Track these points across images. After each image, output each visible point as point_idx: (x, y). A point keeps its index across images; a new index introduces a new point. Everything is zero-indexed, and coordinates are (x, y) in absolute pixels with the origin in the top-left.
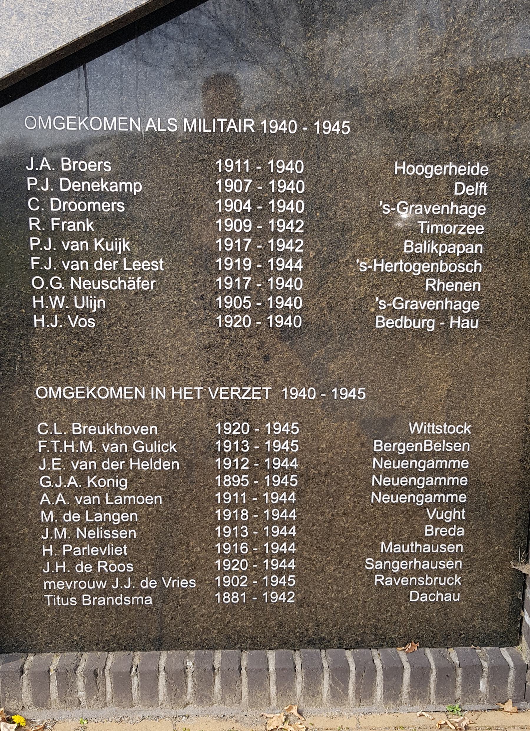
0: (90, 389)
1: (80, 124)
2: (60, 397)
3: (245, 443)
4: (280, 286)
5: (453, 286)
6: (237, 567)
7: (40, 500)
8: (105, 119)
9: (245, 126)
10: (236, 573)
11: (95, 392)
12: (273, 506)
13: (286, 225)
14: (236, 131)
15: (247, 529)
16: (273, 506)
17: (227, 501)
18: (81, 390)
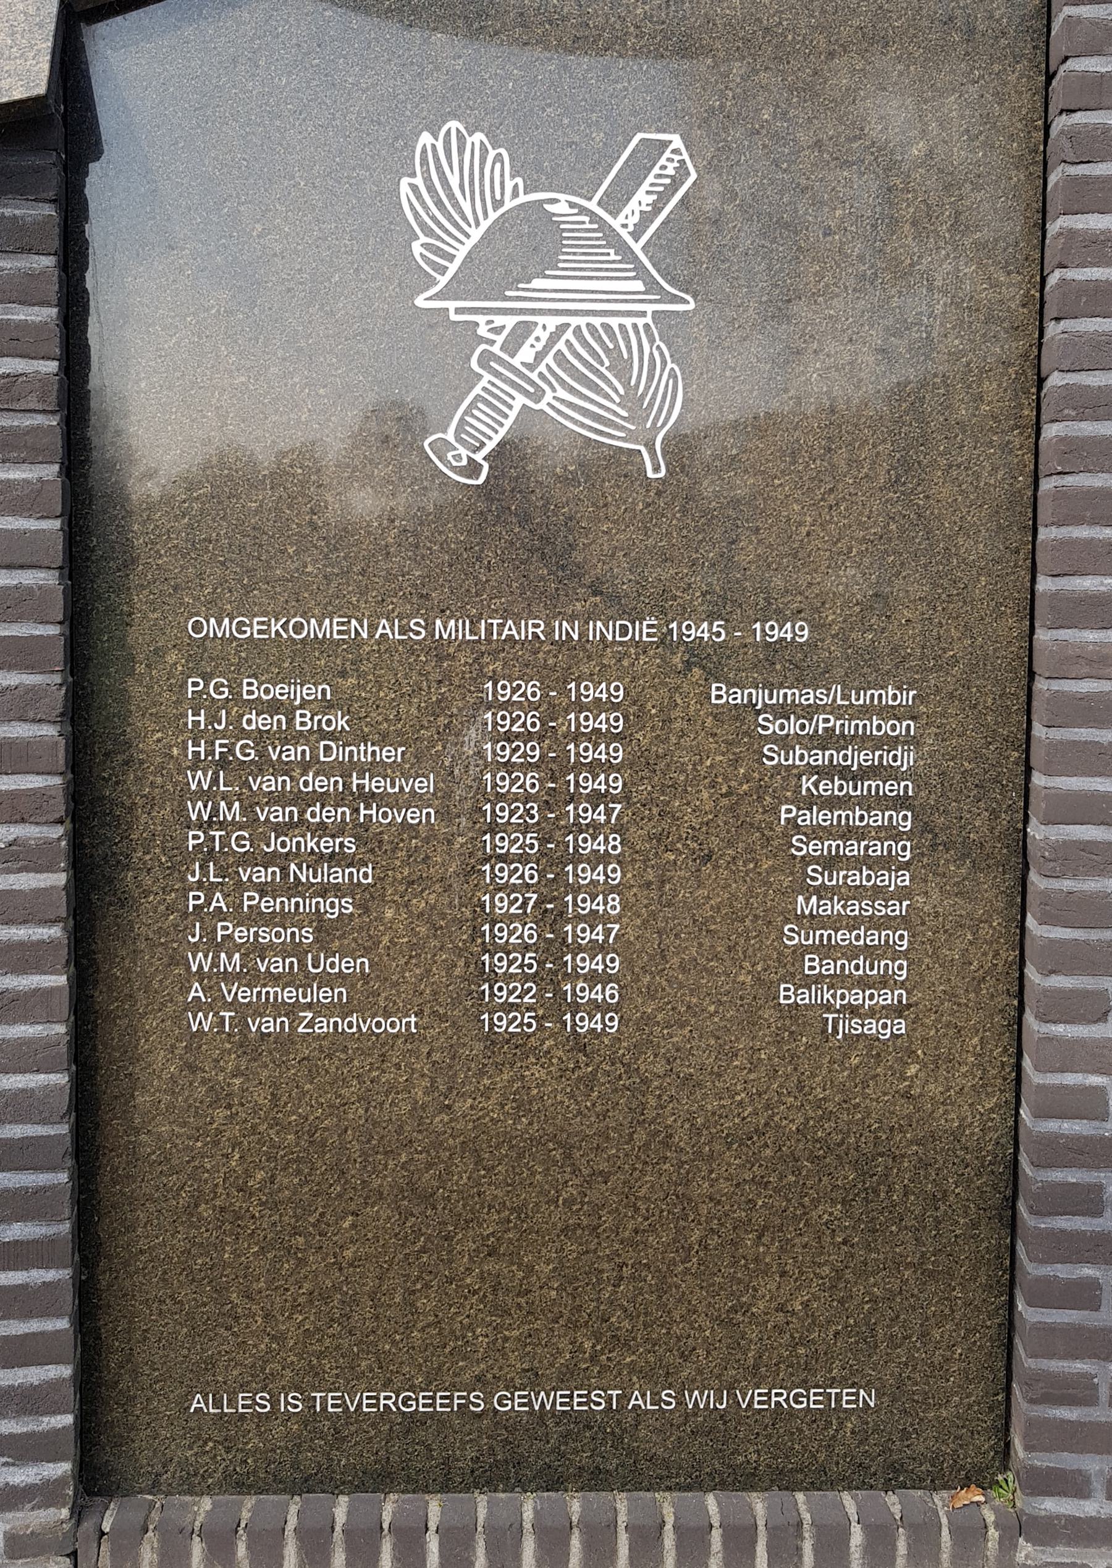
0: (277, 620)
1: (273, 630)
2: (227, 636)
3: (532, 808)
4: (587, 697)
5: (871, 757)
6: (517, 938)
7: (188, 992)
8: (313, 621)
9: (531, 630)
10: (518, 736)
11: (285, 626)
12: (579, 918)
13: (594, 722)
14: (517, 638)
15: (536, 809)
16: (579, 918)
17: (501, 938)
18: (263, 623)
